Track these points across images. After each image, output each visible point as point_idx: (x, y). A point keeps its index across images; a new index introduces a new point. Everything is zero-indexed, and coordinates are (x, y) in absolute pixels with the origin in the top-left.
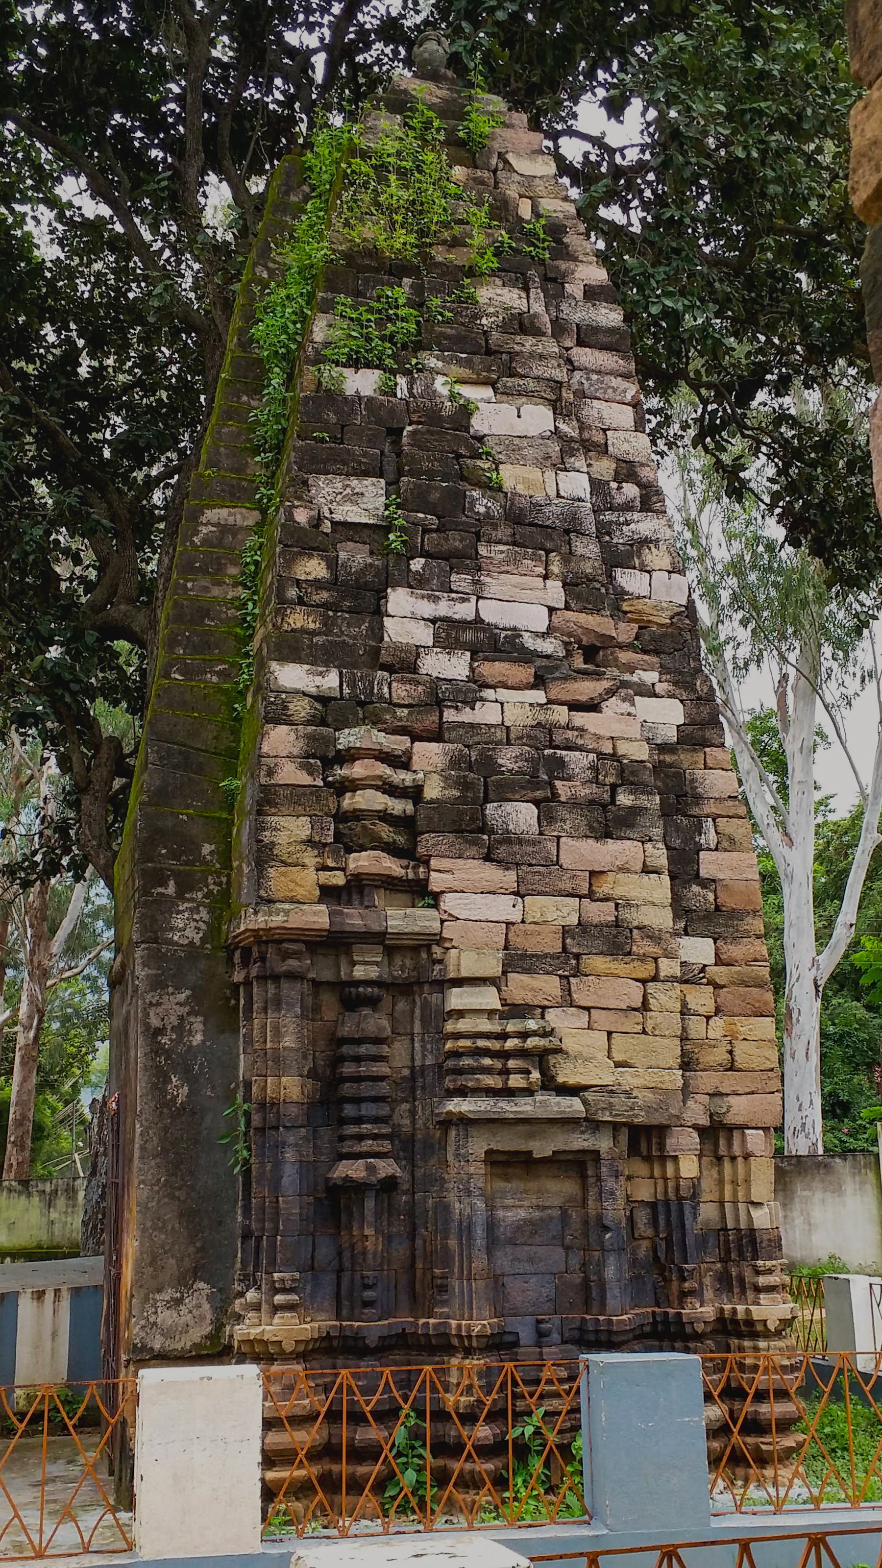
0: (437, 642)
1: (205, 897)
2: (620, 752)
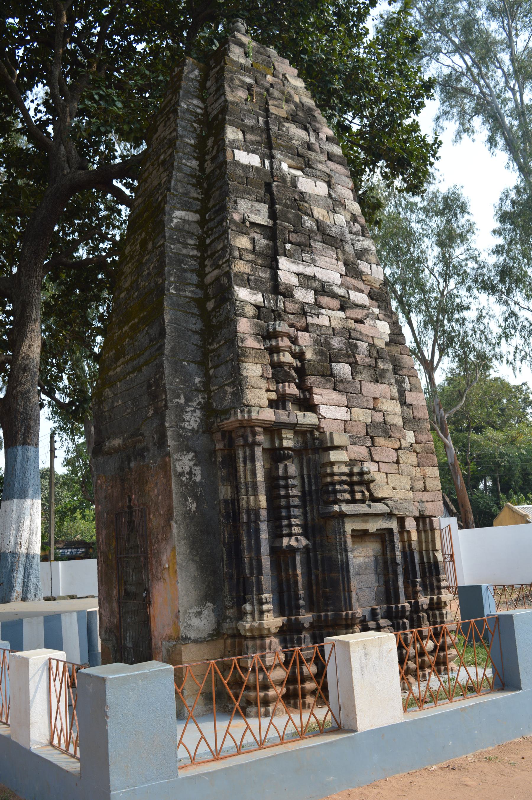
0: (301, 285)
1: (198, 404)
2: (376, 343)
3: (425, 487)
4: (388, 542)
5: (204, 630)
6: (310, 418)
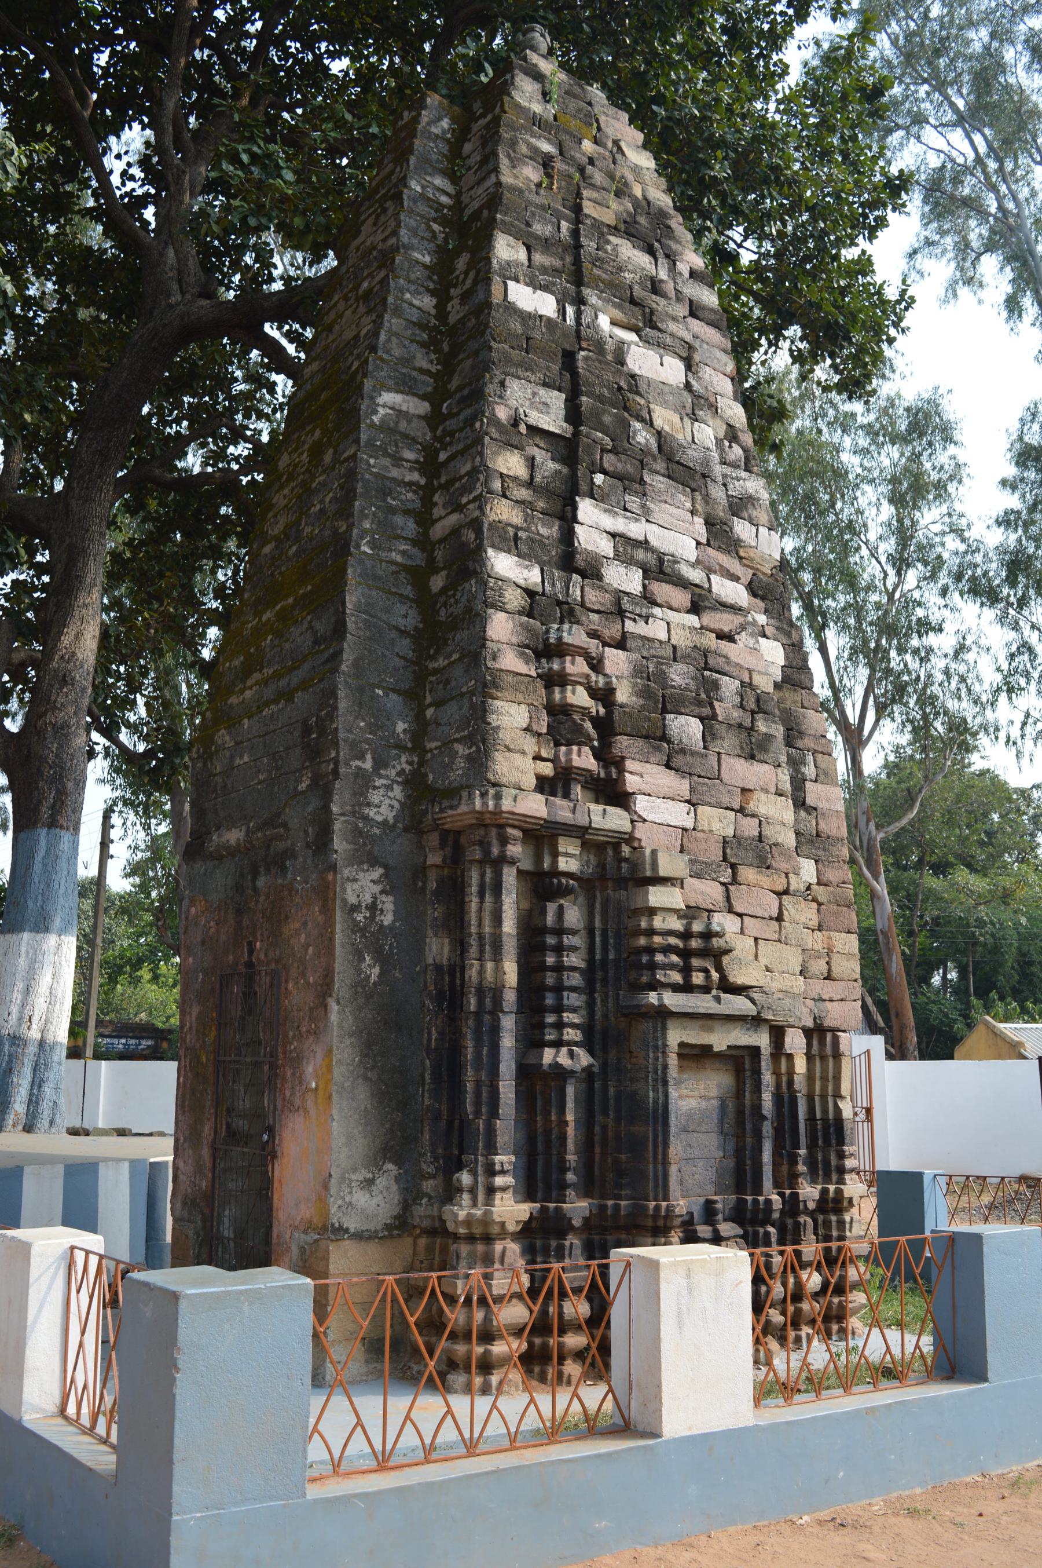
0: (617, 556)
3: (829, 971)
4: (748, 1074)
5: (377, 1215)
6: (615, 819)
